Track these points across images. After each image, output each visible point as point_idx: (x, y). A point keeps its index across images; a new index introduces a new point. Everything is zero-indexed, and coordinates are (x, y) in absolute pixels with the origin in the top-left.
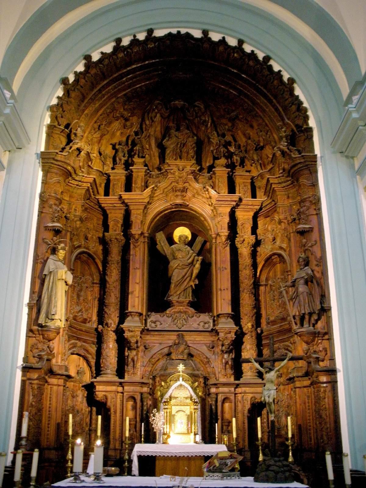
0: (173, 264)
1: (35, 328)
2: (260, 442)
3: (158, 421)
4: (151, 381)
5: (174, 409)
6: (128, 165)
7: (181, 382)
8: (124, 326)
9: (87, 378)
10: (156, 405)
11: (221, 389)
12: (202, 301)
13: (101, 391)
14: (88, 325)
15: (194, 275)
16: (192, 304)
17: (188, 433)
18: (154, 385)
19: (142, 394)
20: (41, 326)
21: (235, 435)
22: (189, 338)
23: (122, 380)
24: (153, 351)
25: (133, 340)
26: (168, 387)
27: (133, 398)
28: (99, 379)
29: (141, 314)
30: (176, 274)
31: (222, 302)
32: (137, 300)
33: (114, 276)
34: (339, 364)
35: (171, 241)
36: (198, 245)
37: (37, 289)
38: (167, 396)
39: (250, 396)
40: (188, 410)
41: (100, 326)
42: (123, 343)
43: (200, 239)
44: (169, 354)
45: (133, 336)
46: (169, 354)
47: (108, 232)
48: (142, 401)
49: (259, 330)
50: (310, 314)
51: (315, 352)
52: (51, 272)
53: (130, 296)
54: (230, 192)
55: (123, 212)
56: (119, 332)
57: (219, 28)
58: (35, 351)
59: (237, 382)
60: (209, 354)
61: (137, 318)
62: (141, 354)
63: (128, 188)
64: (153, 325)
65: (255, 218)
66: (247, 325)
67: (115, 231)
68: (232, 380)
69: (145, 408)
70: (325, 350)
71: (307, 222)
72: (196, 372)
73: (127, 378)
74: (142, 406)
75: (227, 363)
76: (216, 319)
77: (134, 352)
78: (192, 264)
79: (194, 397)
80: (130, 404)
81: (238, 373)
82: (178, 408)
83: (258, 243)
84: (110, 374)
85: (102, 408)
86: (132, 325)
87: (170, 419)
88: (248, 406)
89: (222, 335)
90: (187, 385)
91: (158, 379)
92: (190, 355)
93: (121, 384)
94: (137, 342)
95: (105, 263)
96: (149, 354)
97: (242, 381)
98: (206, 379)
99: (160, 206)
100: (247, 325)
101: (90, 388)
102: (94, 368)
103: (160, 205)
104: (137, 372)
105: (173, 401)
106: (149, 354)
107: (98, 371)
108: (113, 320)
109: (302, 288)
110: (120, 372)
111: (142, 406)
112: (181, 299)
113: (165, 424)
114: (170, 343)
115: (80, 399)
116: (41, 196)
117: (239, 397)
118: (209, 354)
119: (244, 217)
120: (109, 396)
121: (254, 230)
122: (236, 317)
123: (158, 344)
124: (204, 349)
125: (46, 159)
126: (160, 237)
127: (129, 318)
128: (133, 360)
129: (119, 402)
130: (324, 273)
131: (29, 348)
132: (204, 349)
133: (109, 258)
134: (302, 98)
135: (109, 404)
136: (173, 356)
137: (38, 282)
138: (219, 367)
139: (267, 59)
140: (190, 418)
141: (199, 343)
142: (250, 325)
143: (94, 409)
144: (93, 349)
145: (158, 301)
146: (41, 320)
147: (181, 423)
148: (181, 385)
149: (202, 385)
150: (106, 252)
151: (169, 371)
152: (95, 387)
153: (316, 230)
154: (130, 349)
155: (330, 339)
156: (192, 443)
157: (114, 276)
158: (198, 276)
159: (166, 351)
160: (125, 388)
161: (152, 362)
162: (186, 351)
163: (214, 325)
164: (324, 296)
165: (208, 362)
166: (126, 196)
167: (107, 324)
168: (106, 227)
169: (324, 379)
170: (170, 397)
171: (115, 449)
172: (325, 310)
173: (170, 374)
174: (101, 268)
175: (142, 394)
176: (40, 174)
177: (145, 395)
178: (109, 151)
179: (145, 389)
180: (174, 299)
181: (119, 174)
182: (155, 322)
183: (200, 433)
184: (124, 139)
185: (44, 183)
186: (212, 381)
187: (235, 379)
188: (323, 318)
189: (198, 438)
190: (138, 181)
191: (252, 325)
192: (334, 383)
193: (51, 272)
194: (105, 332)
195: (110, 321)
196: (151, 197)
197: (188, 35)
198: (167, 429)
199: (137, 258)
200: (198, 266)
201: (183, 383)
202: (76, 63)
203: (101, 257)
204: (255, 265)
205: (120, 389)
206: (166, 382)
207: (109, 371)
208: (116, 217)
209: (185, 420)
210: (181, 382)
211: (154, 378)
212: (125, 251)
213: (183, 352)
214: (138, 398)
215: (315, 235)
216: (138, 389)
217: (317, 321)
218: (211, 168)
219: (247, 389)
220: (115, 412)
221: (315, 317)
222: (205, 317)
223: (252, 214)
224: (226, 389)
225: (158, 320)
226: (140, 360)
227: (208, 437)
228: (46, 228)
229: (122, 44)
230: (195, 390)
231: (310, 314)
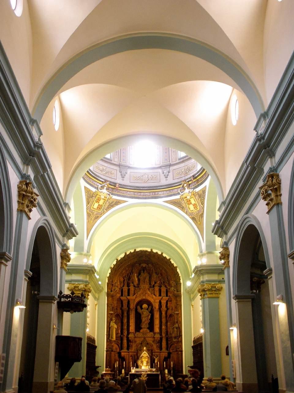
0: (142, 316)
2: (172, 368)
3: (139, 362)
4: (136, 351)
5: (143, 359)
6: (128, 285)
7: (145, 352)
9: (118, 350)
10: (138, 358)
11: (156, 353)
12: (151, 328)
13: (123, 354)
16: (148, 328)
17: (147, 365)
18: (137, 352)
22: (147, 339)
23: (128, 351)
24: (137, 343)
26: (142, 353)
28: (122, 351)
30: (143, 320)
31: (157, 330)
32: (132, 328)
33: (125, 321)
35: (142, 308)
36: (150, 309)
37: (108, 330)
38: (141, 356)
39: (164, 356)
40: (146, 360)
41: (122, 335)
42: (129, 341)
44: (142, 343)
46: (142, 343)
47: (123, 307)
48: (134, 357)
50: (177, 337)
51: (178, 346)
52: (112, 326)
55: (127, 301)
56: (128, 338)
57: (156, 249)
61: (132, 334)
63: (129, 295)
64: (137, 335)
66: (164, 335)
67: (125, 306)
70: (180, 346)
72: (149, 349)
73: (130, 350)
75: (157, 346)
77: (132, 343)
78: (148, 316)
80: (131, 358)
82: (144, 359)
83: (168, 309)
86: (131, 336)
87: (142, 362)
88: (163, 358)
90: (146, 353)
91: (138, 351)
92: (148, 344)
93: (129, 352)
94: (133, 341)
97: (162, 351)
98: (152, 350)
99: (138, 300)
100: (164, 335)
101: (119, 354)
104: (133, 349)
105: (143, 357)
108: (125, 333)
110: (128, 349)
112: (145, 327)
114: (142, 340)
117: (161, 355)
118: (153, 344)
119: (164, 302)
120: (125, 356)
121: (167, 306)
123: (138, 341)
124: (151, 342)
125: (108, 295)
126: (139, 307)
127: (130, 334)
128: (132, 345)
129: (128, 357)
134: (179, 273)
137: (108, 328)
139: (170, 259)
142: (164, 335)
143: (120, 359)
144: (120, 342)
145: (138, 328)
146: (110, 339)
149: (151, 352)
151: (142, 348)
153: (180, 313)
156: (148, 368)
157: (125, 321)
158: (150, 319)
159: (141, 342)
161: (137, 346)
162: (146, 343)
163: (154, 335)
166: (128, 297)
167: (124, 335)
168: (122, 306)
170: (142, 356)
171: (127, 370)
173: (142, 350)
174: (121, 318)
175: (134, 355)
176: (106, 297)
178: (122, 279)
179: (135, 353)
180: (143, 326)
181: (125, 289)
182: (137, 335)
183: (150, 365)
184: (127, 275)
186: (154, 351)
188: (180, 337)
189: (149, 367)
190: (132, 292)
191: (165, 335)
192: (182, 354)
193: (112, 326)
194: (123, 337)
195: (125, 334)
196: (136, 297)
197: (146, 251)
198: (141, 365)
199: (132, 315)
200: (150, 316)
201: (145, 352)
202: (113, 261)
204: (166, 316)
205: (128, 353)
206: (141, 351)
207: (125, 349)
209: (146, 362)
210: (145, 352)
211: (137, 350)
215: (179, 315)
216: (133, 353)
218: (154, 286)
220: (127, 360)
221: (178, 338)
222: (152, 333)
224: (157, 353)
225: (138, 334)
226: (133, 345)
228: (109, 313)
230: (148, 354)
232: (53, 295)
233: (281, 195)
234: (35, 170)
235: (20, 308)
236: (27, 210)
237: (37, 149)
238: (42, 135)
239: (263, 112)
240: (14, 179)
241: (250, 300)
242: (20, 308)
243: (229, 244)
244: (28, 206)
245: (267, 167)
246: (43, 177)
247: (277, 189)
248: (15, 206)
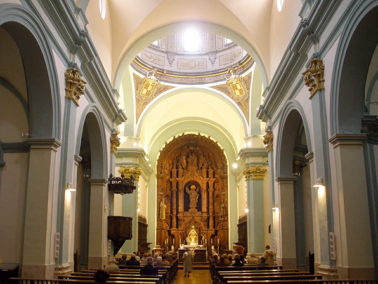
0: (191, 196)
1: (159, 219)
3: (188, 239)
4: (185, 229)
5: (191, 237)
6: (177, 168)
7: (193, 230)
8: (179, 215)
9: (168, 229)
10: (187, 236)
14: (168, 214)
15: (197, 199)
18: (186, 230)
19: (183, 233)
20: (160, 219)
21: (206, 243)
22: (195, 218)
25: (181, 219)
26: (190, 231)
27: (181, 234)
28: (172, 229)
29: (182, 212)
31: (204, 209)
32: (181, 208)
33: (174, 201)
34: (229, 228)
35: (190, 189)
37: (158, 210)
38: (190, 233)
40: (195, 237)
41: (171, 215)
43: (198, 188)
45: (180, 218)
46: (190, 222)
49: (214, 215)
50: (224, 216)
53: (179, 207)
54: (183, 269)
56: (177, 217)
58: (159, 225)
59: (208, 229)
60: (201, 222)
61: (181, 213)
62: (183, 222)
63: (177, 177)
65: (214, 183)
68: (206, 229)
69: (184, 236)
71: (224, 192)
72: (197, 227)
74: (183, 235)
76: (202, 213)
77: (181, 222)
79: (196, 234)
81: (208, 227)
82: (192, 237)
83: (215, 190)
84: (174, 228)
85: (173, 236)
87: (190, 239)
88: (210, 236)
89: (203, 218)
90: (195, 231)
91: (187, 229)
93: (178, 230)
94: (182, 220)
95: (172, 196)
96: (185, 222)
97: (209, 229)
100: (211, 214)
101: (169, 231)
102: (170, 226)
103: (187, 180)
104: (182, 227)
105: (191, 235)
106: (185, 222)
107: (171, 226)
109: (222, 209)
110: (177, 227)
111: (183, 235)
113: (180, 156)
114: (190, 219)
115: (167, 234)
116: (157, 186)
119: (211, 184)
121: (214, 187)
122: (208, 213)
123: (187, 220)
126: (187, 188)
127: (179, 213)
128: (181, 224)
129: (177, 235)
130: (227, 205)
131: (158, 224)
132: (199, 221)
133: (173, 196)
134: (226, 155)
135: (175, 235)
136: (191, 223)
137: (158, 208)
138: (203, 225)
140: (195, 239)
141: (198, 219)
142: (211, 214)
144: (170, 221)
145: (187, 208)
147: (193, 240)
148: (193, 231)
150: (172, 193)
151: (190, 227)
152: (171, 231)
154: (180, 221)
155: (228, 221)
157: (174, 201)
159: (189, 221)
160: (179, 231)
162: (195, 221)
164: (227, 211)
165: (200, 224)
166: (177, 179)
167: (173, 214)
168: (172, 187)
169: (226, 231)
172: (227, 215)
174: (171, 198)
175: (183, 233)
176: (156, 179)
177: (184, 233)
179: (184, 231)
180: (191, 206)
181: (174, 171)
183: (198, 242)
185: (158, 182)
186: (201, 229)
187: (207, 229)
191: (212, 215)
192: (228, 232)
194: (173, 217)
195: (174, 214)
196: (184, 179)
197: (194, 135)
200: (198, 197)
201: (194, 230)
203: (170, 194)
205: (177, 231)
207: (174, 227)
208: (174, 185)
209: (194, 239)
210: (193, 230)
211: (186, 228)
212: (177, 192)
213: (194, 222)
214: (182, 233)
215: (226, 196)
216: (182, 231)
217: (225, 217)
218: (201, 168)
219: (210, 231)
220: (176, 237)
221: (224, 216)
222: (199, 213)
223: (213, 183)
224: (205, 231)
225: (187, 214)
226: (183, 224)
227: (200, 244)
228: (159, 194)
229: (176, 138)
231: (224, 216)
232: (104, 178)
233: (323, 81)
234: (82, 58)
235: (71, 191)
236: (74, 97)
237: (83, 37)
238: (88, 23)
239: (267, 86)
240: (61, 68)
241: (293, 182)
242: (71, 191)
243: (272, 129)
244: (75, 94)
245: (311, 53)
246: (90, 65)
247: (320, 75)
248: (63, 94)
